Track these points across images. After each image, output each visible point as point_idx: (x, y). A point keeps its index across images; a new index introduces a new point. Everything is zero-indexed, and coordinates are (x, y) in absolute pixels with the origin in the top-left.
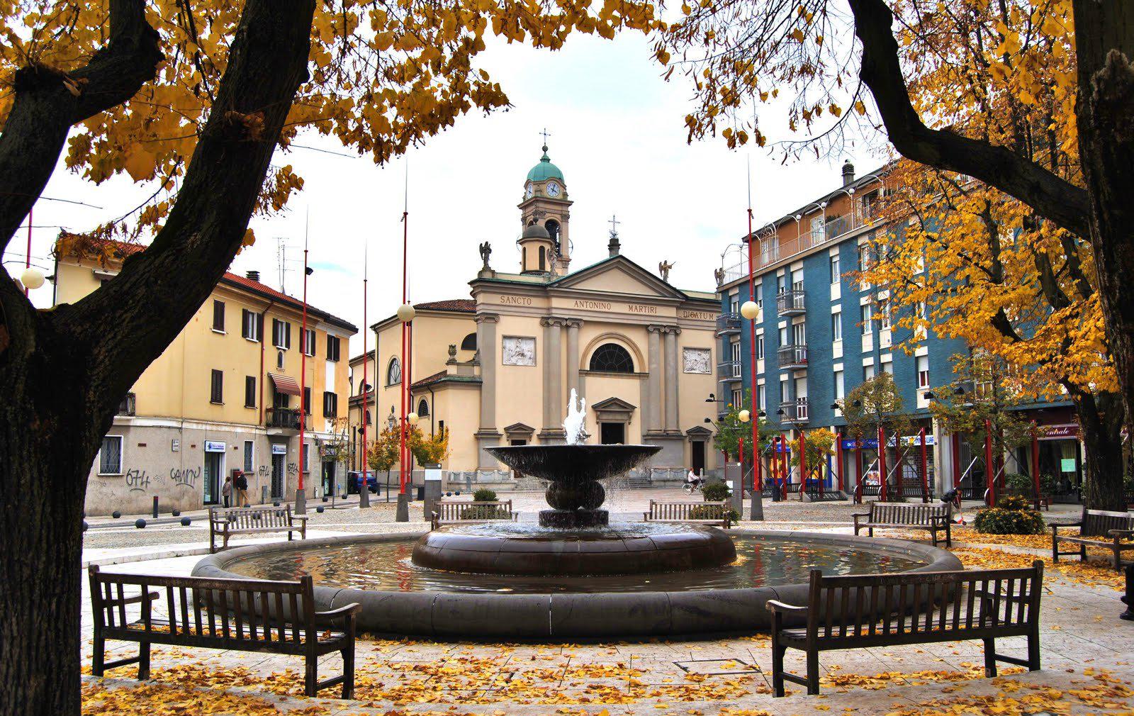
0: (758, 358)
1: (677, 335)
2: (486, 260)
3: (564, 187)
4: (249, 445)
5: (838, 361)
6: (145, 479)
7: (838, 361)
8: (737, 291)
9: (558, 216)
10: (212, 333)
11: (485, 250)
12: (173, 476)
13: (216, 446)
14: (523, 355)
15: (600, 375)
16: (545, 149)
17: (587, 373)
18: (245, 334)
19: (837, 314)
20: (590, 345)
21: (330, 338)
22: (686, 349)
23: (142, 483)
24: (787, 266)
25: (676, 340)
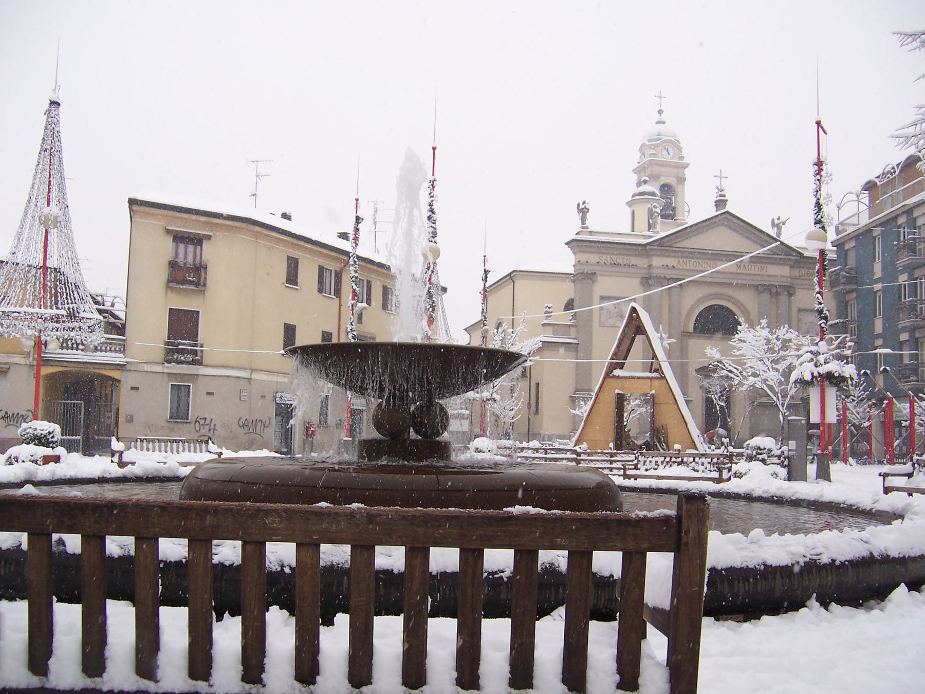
0: (875, 316)
1: (790, 295)
2: (583, 220)
3: (680, 149)
8: (853, 244)
9: (674, 179)
11: (583, 211)
12: (241, 424)
16: (660, 112)
17: (690, 335)
18: (320, 290)
20: (692, 309)
21: (289, 258)
22: (800, 310)
23: (209, 430)
25: (790, 302)
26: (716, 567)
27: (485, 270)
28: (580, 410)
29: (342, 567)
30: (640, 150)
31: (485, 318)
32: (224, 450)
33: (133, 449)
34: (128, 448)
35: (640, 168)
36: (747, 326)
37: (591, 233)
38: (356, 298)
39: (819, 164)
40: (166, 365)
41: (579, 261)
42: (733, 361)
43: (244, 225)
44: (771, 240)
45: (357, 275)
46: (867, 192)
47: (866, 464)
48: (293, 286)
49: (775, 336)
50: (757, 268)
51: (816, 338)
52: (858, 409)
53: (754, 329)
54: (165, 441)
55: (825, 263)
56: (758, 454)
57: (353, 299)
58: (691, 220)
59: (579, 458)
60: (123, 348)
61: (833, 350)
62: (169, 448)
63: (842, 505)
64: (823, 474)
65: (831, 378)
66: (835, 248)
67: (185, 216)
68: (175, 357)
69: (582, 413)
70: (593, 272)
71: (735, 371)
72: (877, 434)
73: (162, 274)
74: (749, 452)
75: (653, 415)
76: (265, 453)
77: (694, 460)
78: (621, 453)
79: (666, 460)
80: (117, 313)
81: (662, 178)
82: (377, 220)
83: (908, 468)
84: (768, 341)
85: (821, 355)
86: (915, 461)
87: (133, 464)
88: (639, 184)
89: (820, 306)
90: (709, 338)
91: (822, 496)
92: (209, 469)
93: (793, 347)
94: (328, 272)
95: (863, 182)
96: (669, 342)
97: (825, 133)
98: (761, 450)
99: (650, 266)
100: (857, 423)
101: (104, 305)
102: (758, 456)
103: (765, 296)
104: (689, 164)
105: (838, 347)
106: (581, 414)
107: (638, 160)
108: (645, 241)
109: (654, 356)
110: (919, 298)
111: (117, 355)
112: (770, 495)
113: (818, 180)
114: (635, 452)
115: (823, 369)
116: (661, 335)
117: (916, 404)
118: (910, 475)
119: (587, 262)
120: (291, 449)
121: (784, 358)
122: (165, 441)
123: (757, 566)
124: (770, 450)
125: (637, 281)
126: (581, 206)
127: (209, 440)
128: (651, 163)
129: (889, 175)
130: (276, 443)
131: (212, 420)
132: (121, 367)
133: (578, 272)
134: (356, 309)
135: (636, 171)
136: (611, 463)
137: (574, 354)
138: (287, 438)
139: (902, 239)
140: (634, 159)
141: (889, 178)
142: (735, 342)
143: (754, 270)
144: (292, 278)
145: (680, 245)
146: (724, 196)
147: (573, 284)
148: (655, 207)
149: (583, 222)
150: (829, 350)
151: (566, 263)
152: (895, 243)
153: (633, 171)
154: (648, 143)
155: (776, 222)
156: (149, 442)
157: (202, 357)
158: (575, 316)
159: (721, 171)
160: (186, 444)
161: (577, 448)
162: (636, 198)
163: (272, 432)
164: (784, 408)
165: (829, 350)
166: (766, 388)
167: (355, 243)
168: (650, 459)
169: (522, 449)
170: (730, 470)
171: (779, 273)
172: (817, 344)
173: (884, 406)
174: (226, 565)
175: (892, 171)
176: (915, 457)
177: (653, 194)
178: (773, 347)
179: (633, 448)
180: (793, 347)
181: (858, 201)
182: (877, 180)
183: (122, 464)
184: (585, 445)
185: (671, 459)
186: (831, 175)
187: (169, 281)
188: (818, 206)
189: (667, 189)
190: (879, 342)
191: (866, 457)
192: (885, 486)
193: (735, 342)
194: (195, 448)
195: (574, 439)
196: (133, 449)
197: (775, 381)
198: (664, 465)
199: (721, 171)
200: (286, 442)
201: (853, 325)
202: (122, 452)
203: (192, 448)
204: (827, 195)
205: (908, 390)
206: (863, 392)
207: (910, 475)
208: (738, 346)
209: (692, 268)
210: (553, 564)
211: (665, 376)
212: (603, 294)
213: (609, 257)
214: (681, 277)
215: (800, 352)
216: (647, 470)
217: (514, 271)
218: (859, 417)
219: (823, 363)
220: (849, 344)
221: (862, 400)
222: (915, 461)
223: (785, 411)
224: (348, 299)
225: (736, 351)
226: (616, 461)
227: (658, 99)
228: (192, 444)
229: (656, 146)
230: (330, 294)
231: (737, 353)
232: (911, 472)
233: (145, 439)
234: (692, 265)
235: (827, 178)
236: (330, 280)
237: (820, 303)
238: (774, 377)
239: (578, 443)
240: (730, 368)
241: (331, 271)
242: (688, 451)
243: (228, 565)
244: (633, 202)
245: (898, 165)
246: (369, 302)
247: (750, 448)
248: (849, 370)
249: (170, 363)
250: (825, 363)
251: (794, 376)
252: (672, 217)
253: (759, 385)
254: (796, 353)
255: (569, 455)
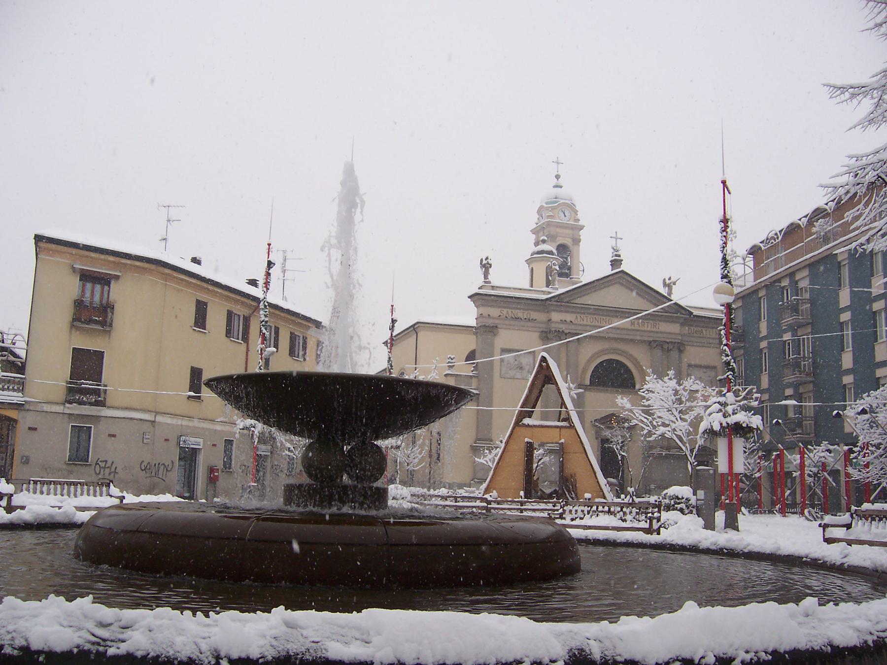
1: (681, 351)
3: (576, 212)
4: (229, 443)
5: (848, 372)
6: (113, 469)
7: (848, 372)
10: (191, 331)
11: (486, 266)
12: (143, 468)
13: (193, 442)
14: (521, 368)
15: (601, 391)
16: (558, 177)
18: (229, 333)
19: (846, 323)
20: (589, 361)
21: (198, 302)
22: (690, 366)
23: (110, 474)
24: (792, 275)
25: (680, 358)
26: (778, 650)
27: (392, 319)
28: (485, 459)
29: (301, 659)
30: (538, 212)
31: (391, 366)
32: (125, 494)
33: (25, 492)
34: (19, 490)
35: (538, 228)
36: (655, 377)
37: (493, 288)
38: (265, 342)
39: (725, 221)
40: (67, 405)
41: (481, 314)
42: (643, 411)
43: (153, 267)
44: (665, 300)
45: (267, 319)
46: (752, 256)
47: (757, 514)
48: (201, 330)
49: (682, 387)
50: (650, 325)
51: (723, 389)
52: (749, 460)
53: (662, 380)
54: (62, 484)
55: (732, 317)
56: (676, 503)
57: (263, 343)
58: (585, 279)
59: (489, 506)
60: (21, 386)
61: (740, 401)
62: (65, 491)
63: (804, 559)
64: (731, 524)
65: (738, 429)
66: (722, 308)
67: (93, 255)
68: (77, 398)
69: (486, 461)
70: (495, 325)
71: (645, 420)
72: (765, 484)
73: (67, 313)
74: (667, 501)
75: (562, 466)
76: (168, 498)
77: (622, 510)
78: (532, 502)
79: (592, 510)
80: (18, 351)
81: (558, 238)
82: (287, 268)
83: (845, 518)
84: (676, 392)
85: (729, 406)
86: (853, 512)
87: (23, 508)
88: (537, 244)
89: (727, 358)
90: (38, 515)
91: (779, 549)
92: (111, 516)
93: (701, 398)
94: (236, 318)
95: (749, 246)
96: (575, 392)
97: (729, 193)
98: (679, 499)
99: (550, 320)
100: (748, 474)
101: (3, 342)
102: (676, 506)
103: (658, 352)
104: (584, 226)
105: (745, 398)
106: (485, 463)
107: (536, 220)
108: (545, 297)
109: (563, 404)
110: (802, 356)
111: (15, 394)
112: (719, 547)
113: (725, 236)
114: (561, 501)
115: (732, 420)
116: (569, 385)
117: (806, 456)
118: (848, 526)
119: (489, 315)
120: (194, 494)
121: (691, 409)
122: (62, 484)
123: (823, 647)
124: (688, 500)
125: (536, 335)
126: (484, 262)
127: (111, 484)
128: (549, 224)
129: (773, 241)
130: (178, 487)
131: (113, 462)
132: (18, 406)
133: (479, 325)
134: (265, 354)
135: (534, 231)
136: (522, 512)
137: (476, 403)
138: (189, 483)
139: (785, 301)
140: (532, 220)
141: (772, 243)
142: (644, 392)
143: (648, 327)
144: (200, 320)
145: (578, 301)
146: (619, 256)
147: (475, 336)
148: (554, 264)
149: (486, 277)
150: (736, 401)
151: (469, 316)
152: (780, 303)
153: (531, 231)
154: (545, 205)
155: (668, 282)
156: (44, 484)
157: (105, 398)
158: (476, 368)
159: (616, 233)
160: (85, 487)
161: (487, 496)
162: (535, 256)
163: (175, 476)
164: (693, 458)
165: (736, 401)
166: (675, 438)
167: (266, 287)
168: (576, 508)
169: (432, 496)
170: (659, 520)
171: (672, 329)
172: (724, 395)
173: (773, 457)
174: (136, 657)
175: (775, 237)
176: (853, 508)
177: (551, 253)
178: (680, 398)
179: (544, 497)
180: (701, 398)
181: (744, 264)
182: (761, 245)
183: (10, 509)
184: (495, 493)
185: (597, 508)
186: (735, 233)
187: (74, 320)
188: (725, 261)
189: (563, 249)
190: (789, 392)
191: (756, 506)
192: (826, 537)
193: (644, 392)
194: (95, 492)
195: (484, 485)
196: (25, 492)
197: (684, 431)
198: (590, 514)
199: (616, 233)
200: (189, 487)
201: (740, 381)
202: (12, 495)
203: (92, 491)
204: (732, 251)
205: (798, 441)
206: (754, 444)
207: (848, 526)
208: (647, 396)
209: (589, 323)
210: (582, 650)
211: (574, 426)
212: (505, 347)
213: (510, 311)
214: (578, 332)
215: (708, 403)
216: (572, 520)
217: (418, 323)
218: (751, 469)
219: (731, 413)
220: (756, 395)
221: (753, 451)
222: (853, 512)
223: (694, 461)
224: (256, 343)
225: (645, 401)
226: (526, 510)
227: (555, 165)
228: (92, 488)
229: (553, 208)
230: (238, 339)
231: (647, 403)
232: (850, 522)
233: (39, 481)
234: (589, 320)
235: (731, 236)
236: (238, 325)
237: (727, 356)
238: (682, 427)
239: (487, 491)
240: (640, 417)
241: (239, 316)
242: (597, 500)
243: (139, 657)
244: (533, 259)
245: (780, 231)
246: (276, 346)
247: (667, 498)
248: (756, 421)
249: (71, 403)
250: (733, 414)
251: (703, 426)
252: (567, 275)
253: (669, 435)
254: (704, 403)
255: (478, 503)
